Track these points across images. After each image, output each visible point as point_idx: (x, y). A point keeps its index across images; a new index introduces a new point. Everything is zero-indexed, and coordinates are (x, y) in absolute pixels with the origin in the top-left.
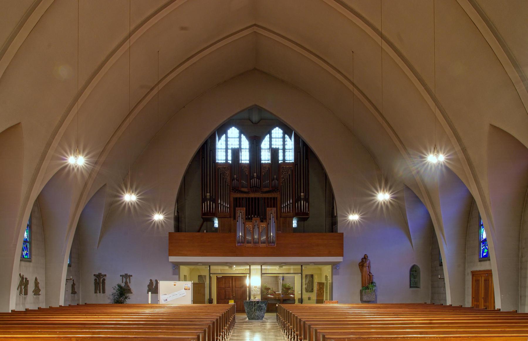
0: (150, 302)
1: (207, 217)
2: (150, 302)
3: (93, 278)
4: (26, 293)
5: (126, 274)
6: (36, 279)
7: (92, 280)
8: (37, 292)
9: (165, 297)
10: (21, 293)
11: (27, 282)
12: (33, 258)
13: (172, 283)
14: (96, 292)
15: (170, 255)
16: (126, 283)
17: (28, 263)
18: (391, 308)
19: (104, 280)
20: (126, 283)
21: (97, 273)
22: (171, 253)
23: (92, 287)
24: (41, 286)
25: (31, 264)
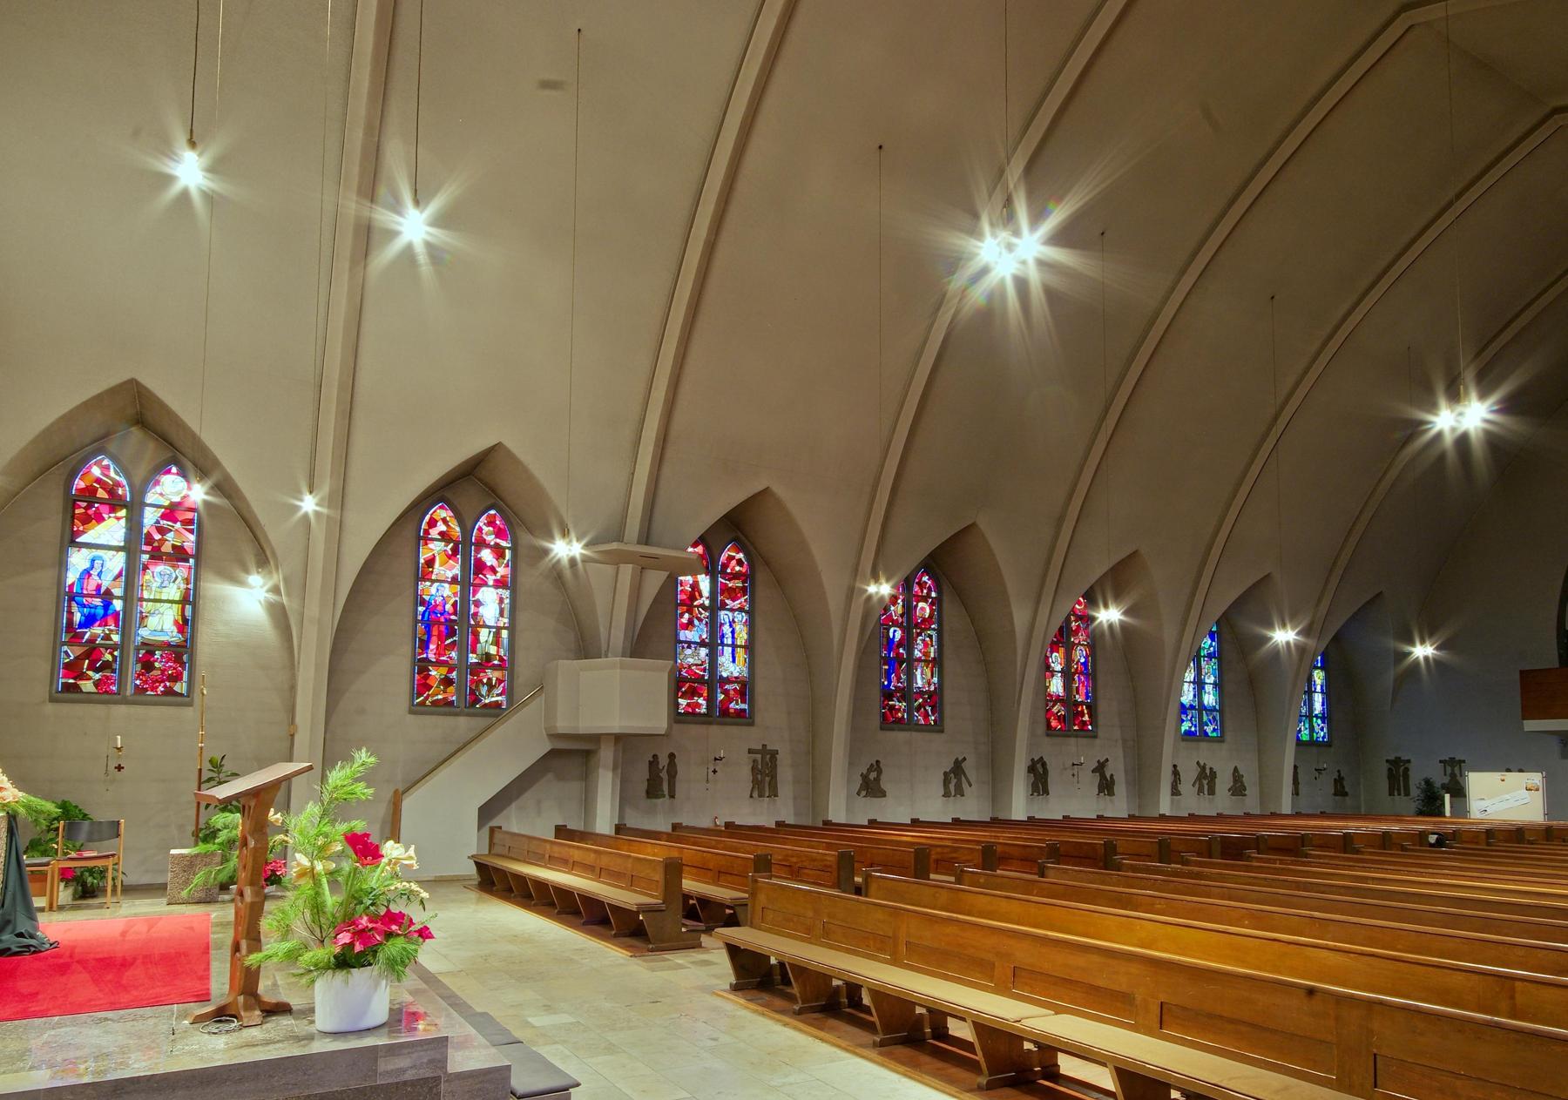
0: (173, 852)
1: (112, 693)
2: (173, 852)
3: (1386, 766)
4: (1212, 792)
5: (1452, 759)
6: (1236, 769)
7: (1384, 768)
8: (1238, 789)
9: (1483, 805)
10: (1200, 791)
11: (1213, 774)
12: (1228, 737)
13: (1497, 776)
14: (1391, 794)
15: (1524, 718)
16: (1453, 775)
17: (1216, 745)
18: (521, 879)
19: (1407, 770)
20: (1453, 775)
21: (1392, 757)
22: (1528, 714)
23: (1384, 784)
24: (1250, 779)
25: (1224, 746)
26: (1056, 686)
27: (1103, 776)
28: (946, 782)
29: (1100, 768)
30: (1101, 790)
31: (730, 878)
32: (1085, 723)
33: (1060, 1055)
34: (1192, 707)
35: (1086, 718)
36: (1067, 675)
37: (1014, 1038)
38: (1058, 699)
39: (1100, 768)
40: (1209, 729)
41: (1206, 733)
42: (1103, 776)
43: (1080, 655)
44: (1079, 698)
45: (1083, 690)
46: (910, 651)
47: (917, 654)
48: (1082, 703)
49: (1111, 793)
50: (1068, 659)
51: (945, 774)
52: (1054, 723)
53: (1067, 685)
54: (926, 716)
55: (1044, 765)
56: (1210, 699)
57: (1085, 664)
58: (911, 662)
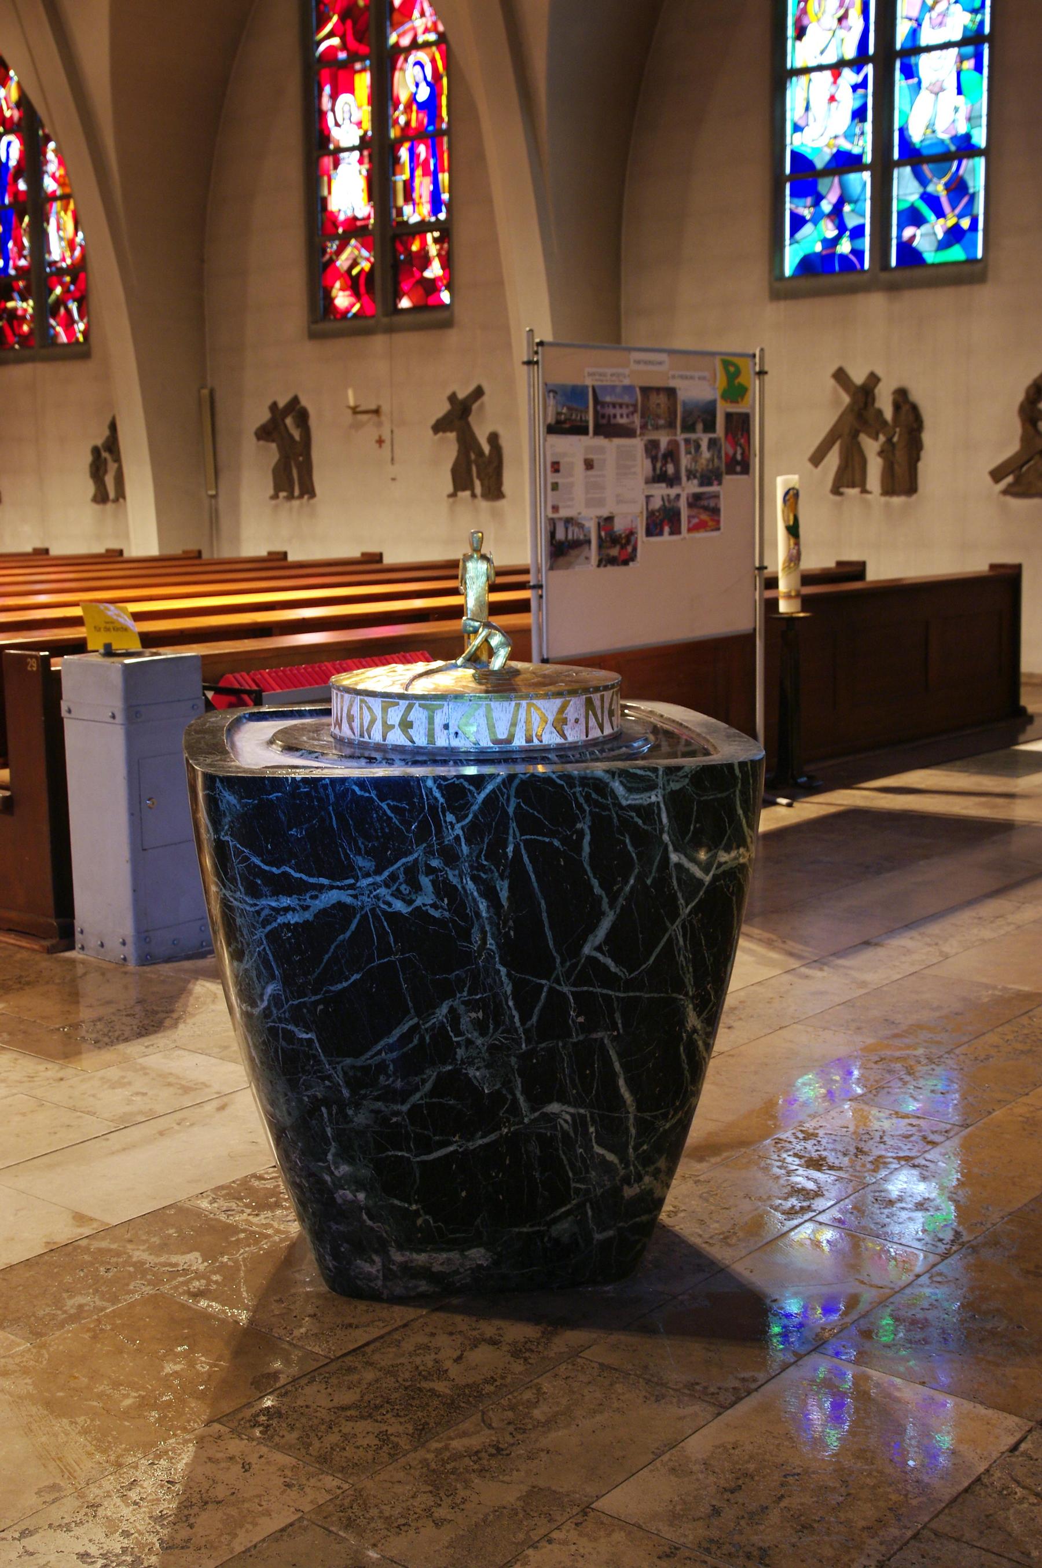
4: (902, 480)
10: (852, 474)
26: (348, 193)
27: (467, 442)
28: (97, 470)
29: (458, 417)
30: (461, 480)
31: (192, 555)
32: (432, 287)
33: (650, 508)
34: (845, 162)
35: (434, 270)
36: (379, 152)
37: (444, 778)
38: (354, 228)
39: (458, 417)
40: (925, 238)
41: (909, 254)
42: (467, 442)
43: (410, 81)
44: (413, 215)
45: (423, 186)
46: (36, 178)
47: (50, 185)
48: (423, 228)
49: (494, 491)
50: (382, 98)
51: (96, 451)
52: (342, 299)
53: (379, 187)
54: (69, 323)
55: (303, 418)
56: (941, 104)
57: (430, 106)
58: (38, 205)
